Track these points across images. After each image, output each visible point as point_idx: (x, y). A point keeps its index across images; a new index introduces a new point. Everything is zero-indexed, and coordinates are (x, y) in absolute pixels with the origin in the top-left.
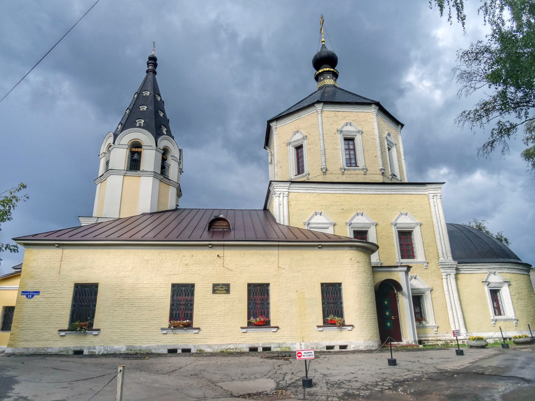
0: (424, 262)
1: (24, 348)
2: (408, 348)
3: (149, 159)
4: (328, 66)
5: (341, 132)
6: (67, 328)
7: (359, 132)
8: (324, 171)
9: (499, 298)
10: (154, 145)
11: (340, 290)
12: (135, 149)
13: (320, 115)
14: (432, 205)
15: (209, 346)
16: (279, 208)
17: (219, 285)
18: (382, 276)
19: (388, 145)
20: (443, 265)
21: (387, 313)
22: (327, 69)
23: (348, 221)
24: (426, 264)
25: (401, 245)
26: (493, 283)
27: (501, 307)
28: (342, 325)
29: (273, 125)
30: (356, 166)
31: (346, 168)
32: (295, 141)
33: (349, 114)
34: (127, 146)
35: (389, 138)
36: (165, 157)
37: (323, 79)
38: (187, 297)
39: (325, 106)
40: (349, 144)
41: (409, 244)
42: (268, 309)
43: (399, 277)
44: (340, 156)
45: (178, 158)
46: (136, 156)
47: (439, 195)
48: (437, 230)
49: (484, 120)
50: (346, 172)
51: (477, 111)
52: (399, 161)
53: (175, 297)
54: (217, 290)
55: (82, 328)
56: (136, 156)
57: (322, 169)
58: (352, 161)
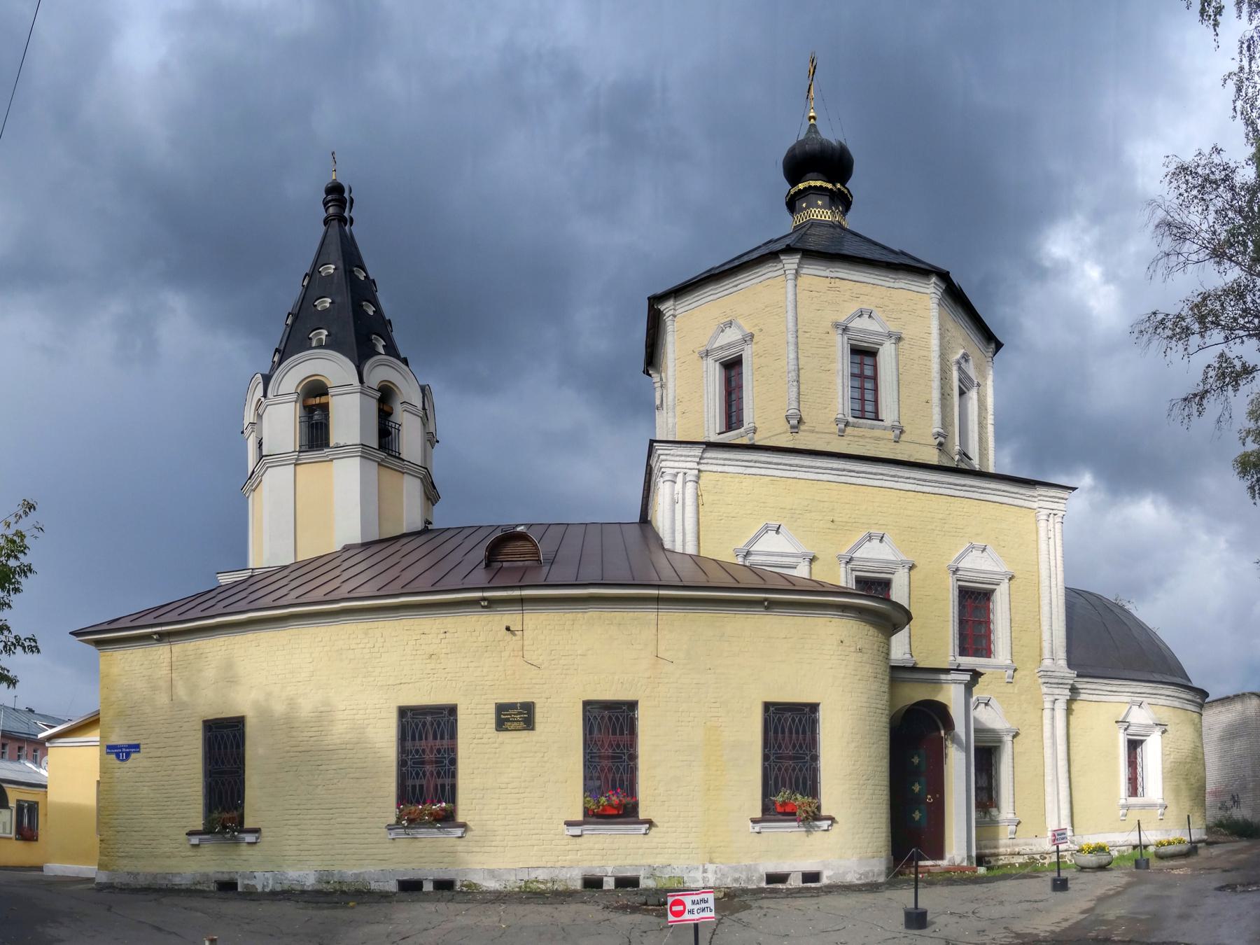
0: (1007, 668)
1: (128, 873)
2: (954, 878)
3: (349, 417)
4: (820, 176)
5: (845, 329)
6: (201, 828)
7: (890, 335)
8: (794, 422)
9: (1139, 760)
10: (356, 381)
11: (814, 723)
12: (314, 402)
13: (790, 284)
14: (1042, 534)
15: (492, 874)
16: (675, 519)
17: (512, 706)
18: (915, 693)
19: (960, 380)
20: (1050, 677)
21: (917, 788)
22: (818, 183)
23: (844, 552)
24: (1011, 672)
25: (962, 622)
26: (1136, 725)
27: (1140, 779)
28: (813, 817)
29: (667, 307)
30: (877, 419)
31: (851, 419)
32: (721, 348)
33: (868, 289)
34: (295, 396)
35: (964, 365)
36: (386, 408)
37: (807, 207)
38: (438, 742)
39: (804, 261)
40: (862, 364)
41: (980, 623)
42: (633, 771)
43: (952, 695)
44: (835, 394)
45: (420, 406)
46: (317, 416)
47: (1060, 514)
48: (1047, 594)
49: (1195, 340)
50: (849, 430)
51: (1180, 317)
52: (982, 426)
53: (409, 744)
54: (508, 720)
55: (225, 827)
56: (317, 416)
57: (787, 418)
58: (866, 401)
